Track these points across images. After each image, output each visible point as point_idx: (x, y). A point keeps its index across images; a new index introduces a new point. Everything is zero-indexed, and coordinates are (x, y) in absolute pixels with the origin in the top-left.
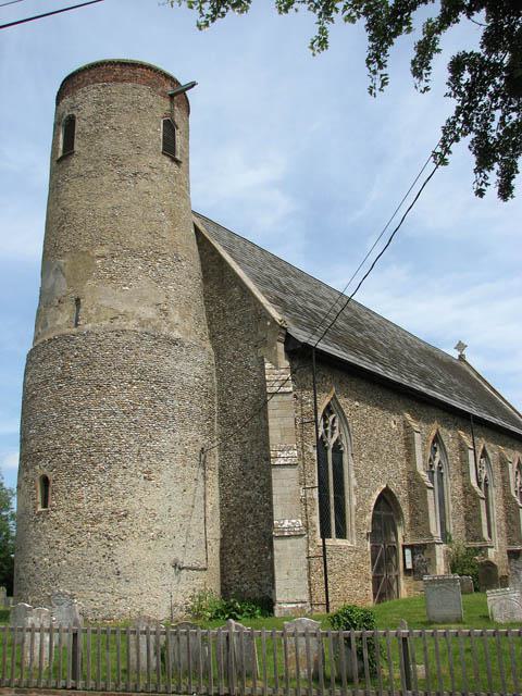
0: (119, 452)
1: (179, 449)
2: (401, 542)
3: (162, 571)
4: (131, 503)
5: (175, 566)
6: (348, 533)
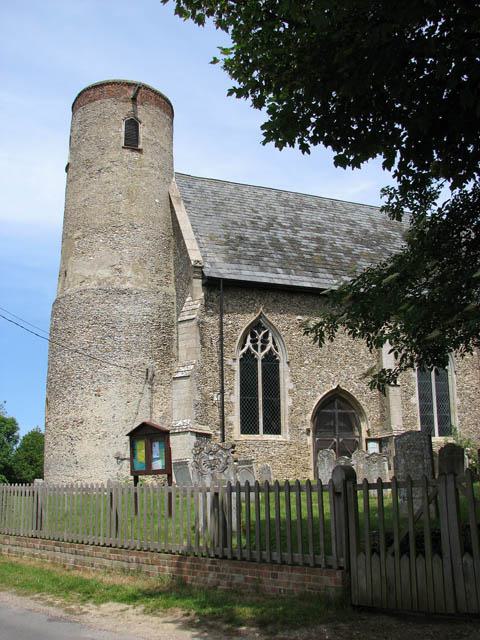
0: (79, 378)
1: (377, 379)
2: (364, 435)
3: (106, 462)
4: (86, 414)
5: (118, 458)
6: (283, 430)
